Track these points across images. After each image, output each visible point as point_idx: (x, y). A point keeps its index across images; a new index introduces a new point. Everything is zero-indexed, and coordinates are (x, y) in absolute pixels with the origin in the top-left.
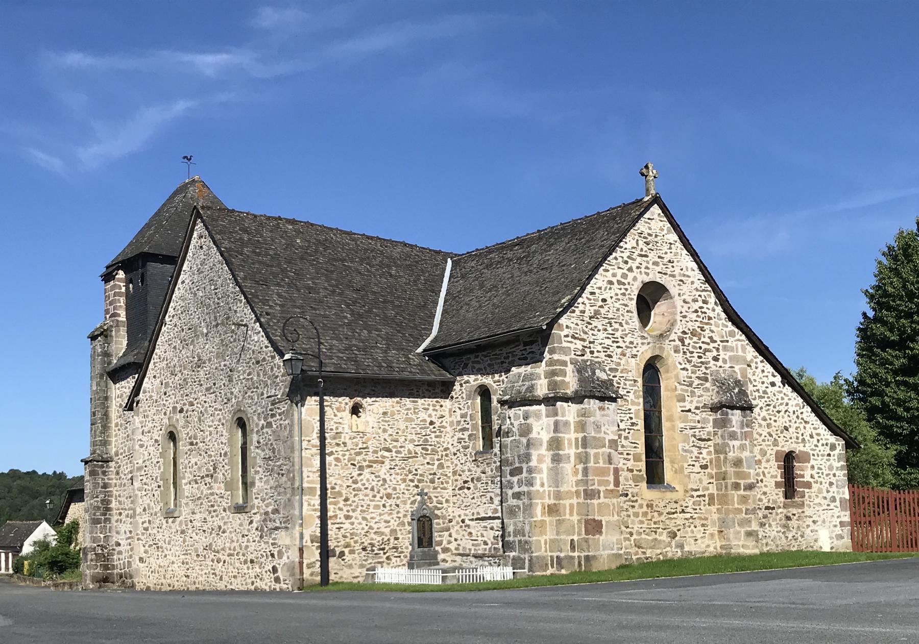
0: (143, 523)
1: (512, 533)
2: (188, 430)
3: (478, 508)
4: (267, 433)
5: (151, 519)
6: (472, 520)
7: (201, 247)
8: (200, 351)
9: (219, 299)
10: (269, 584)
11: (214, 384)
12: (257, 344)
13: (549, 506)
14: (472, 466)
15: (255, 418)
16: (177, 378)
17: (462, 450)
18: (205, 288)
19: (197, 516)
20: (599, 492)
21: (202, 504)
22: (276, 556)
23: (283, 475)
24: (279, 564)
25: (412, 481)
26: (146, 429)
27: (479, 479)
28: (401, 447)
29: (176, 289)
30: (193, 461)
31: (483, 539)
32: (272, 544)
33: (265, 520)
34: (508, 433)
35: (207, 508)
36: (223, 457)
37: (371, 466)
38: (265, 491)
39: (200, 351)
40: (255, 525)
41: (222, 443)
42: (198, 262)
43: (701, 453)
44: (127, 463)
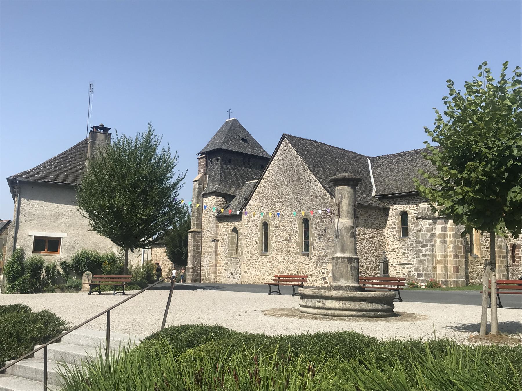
0: (247, 257)
1: (421, 270)
2: (275, 221)
3: (400, 260)
4: (321, 225)
5: (252, 256)
6: (397, 264)
7: (285, 151)
8: (283, 191)
9: (294, 171)
10: (321, 284)
11: (291, 204)
12: (316, 190)
13: (438, 260)
14: (398, 242)
15: (314, 219)
16: (269, 201)
17: (392, 236)
18: (286, 167)
19: (280, 256)
20: (458, 256)
21: (282, 251)
22: (325, 273)
23: (329, 242)
24: (327, 277)
25: (373, 247)
26: (250, 220)
27: (401, 248)
28: (370, 233)
29: (270, 166)
30: (277, 234)
31: (403, 272)
32: (323, 269)
33: (319, 259)
34: (420, 230)
35: (285, 253)
36: (295, 233)
37: (361, 240)
38: (319, 247)
39: (283, 191)
40: (313, 261)
41: (294, 227)
42: (283, 156)
43: (487, 243)
44: (208, 233)
